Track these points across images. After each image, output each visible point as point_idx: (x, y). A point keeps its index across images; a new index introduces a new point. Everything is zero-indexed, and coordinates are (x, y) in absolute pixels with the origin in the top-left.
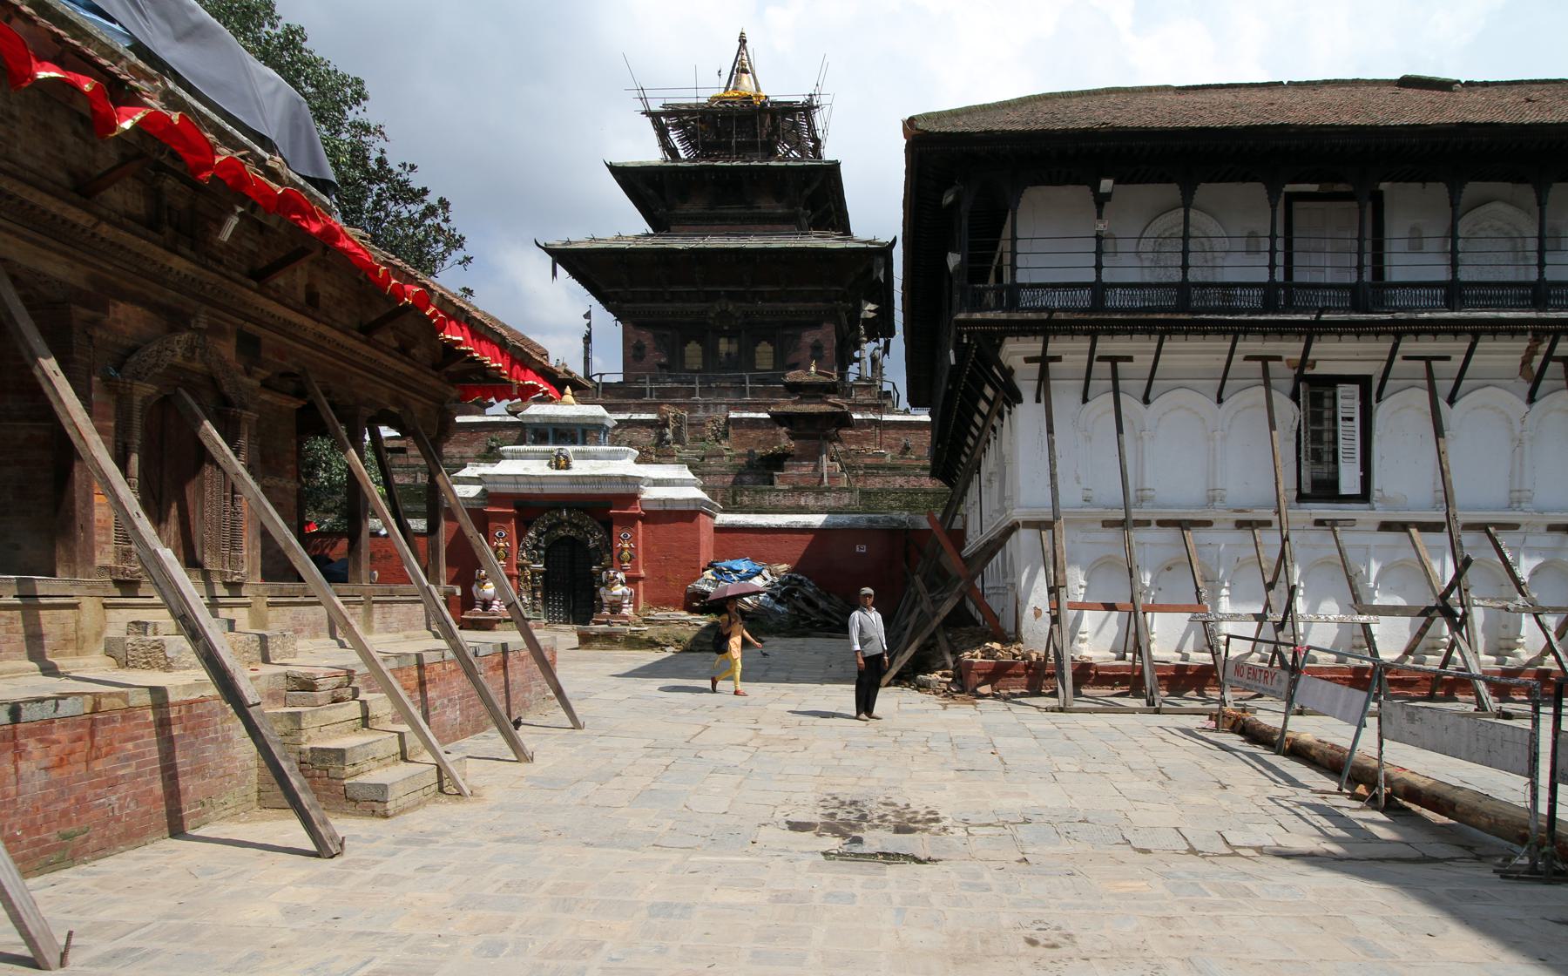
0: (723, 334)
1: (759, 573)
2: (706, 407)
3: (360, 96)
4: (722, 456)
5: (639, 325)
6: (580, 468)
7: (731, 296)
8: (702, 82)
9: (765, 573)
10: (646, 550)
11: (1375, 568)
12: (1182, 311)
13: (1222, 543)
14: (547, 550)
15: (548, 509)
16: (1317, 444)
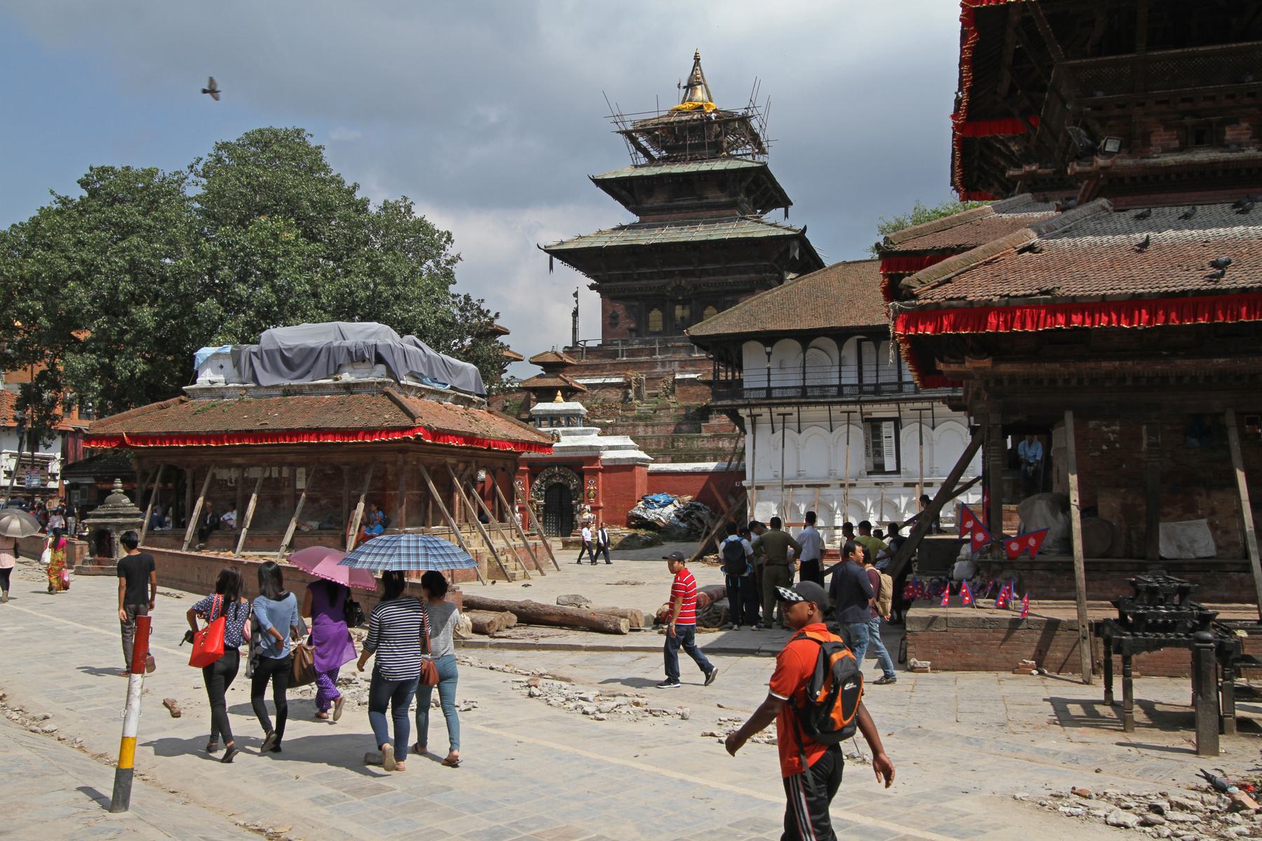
0: (678, 303)
1: (671, 503)
2: (663, 363)
3: (449, 239)
4: (668, 408)
5: (614, 299)
6: (566, 441)
7: (683, 274)
8: (664, 102)
9: (676, 502)
10: (604, 490)
11: (869, 503)
12: (805, 396)
13: (835, 492)
14: (546, 491)
15: (547, 467)
16: (875, 447)
